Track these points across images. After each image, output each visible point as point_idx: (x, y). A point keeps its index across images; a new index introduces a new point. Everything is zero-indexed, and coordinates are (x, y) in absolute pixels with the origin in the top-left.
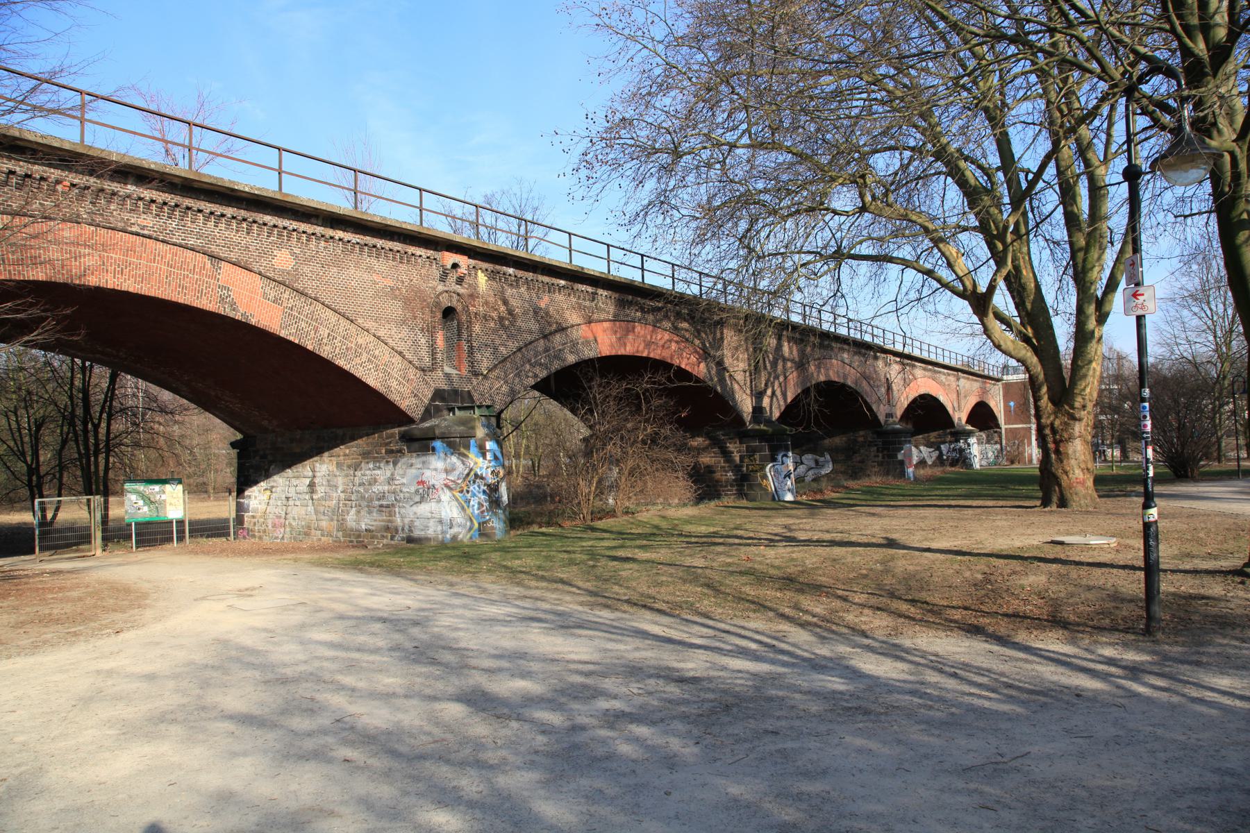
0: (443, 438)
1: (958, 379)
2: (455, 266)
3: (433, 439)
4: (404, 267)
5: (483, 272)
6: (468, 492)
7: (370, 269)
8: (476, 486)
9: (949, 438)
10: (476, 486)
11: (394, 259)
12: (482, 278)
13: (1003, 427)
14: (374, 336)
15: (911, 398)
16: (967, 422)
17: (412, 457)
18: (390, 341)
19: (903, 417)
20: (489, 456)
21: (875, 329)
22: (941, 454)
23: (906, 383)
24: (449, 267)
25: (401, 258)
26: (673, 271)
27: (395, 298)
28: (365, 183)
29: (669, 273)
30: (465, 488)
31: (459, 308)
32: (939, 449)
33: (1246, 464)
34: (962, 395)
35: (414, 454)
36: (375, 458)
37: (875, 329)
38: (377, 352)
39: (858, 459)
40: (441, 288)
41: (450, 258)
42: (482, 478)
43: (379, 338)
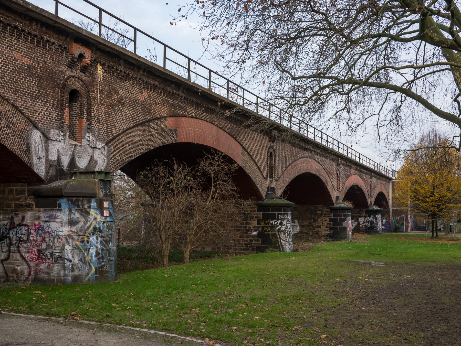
0: (69, 197)
1: (371, 178)
2: (81, 56)
3: (62, 197)
4: (39, 50)
5: (101, 65)
6: (88, 242)
7: (10, 46)
8: (94, 237)
9: (364, 214)
10: (94, 237)
11: (32, 42)
12: (100, 71)
13: (391, 208)
14: (13, 105)
15: (293, 176)
16: (375, 204)
17: (39, 211)
18: (26, 111)
19: (285, 193)
20: (106, 213)
21: (192, 64)
22: (359, 224)
23: (348, 177)
24: (76, 56)
25: (38, 42)
26: (348, 149)
27: (32, 75)
28: (106, 19)
29: (207, 75)
30: (86, 239)
31: (82, 92)
32: (357, 220)
33: (325, 0)
34: (373, 187)
35: (42, 209)
36: (4, 210)
37: (192, 64)
38: (15, 120)
39: (317, 225)
40: (68, 73)
41: (77, 50)
42: (101, 231)
43: (17, 108)
